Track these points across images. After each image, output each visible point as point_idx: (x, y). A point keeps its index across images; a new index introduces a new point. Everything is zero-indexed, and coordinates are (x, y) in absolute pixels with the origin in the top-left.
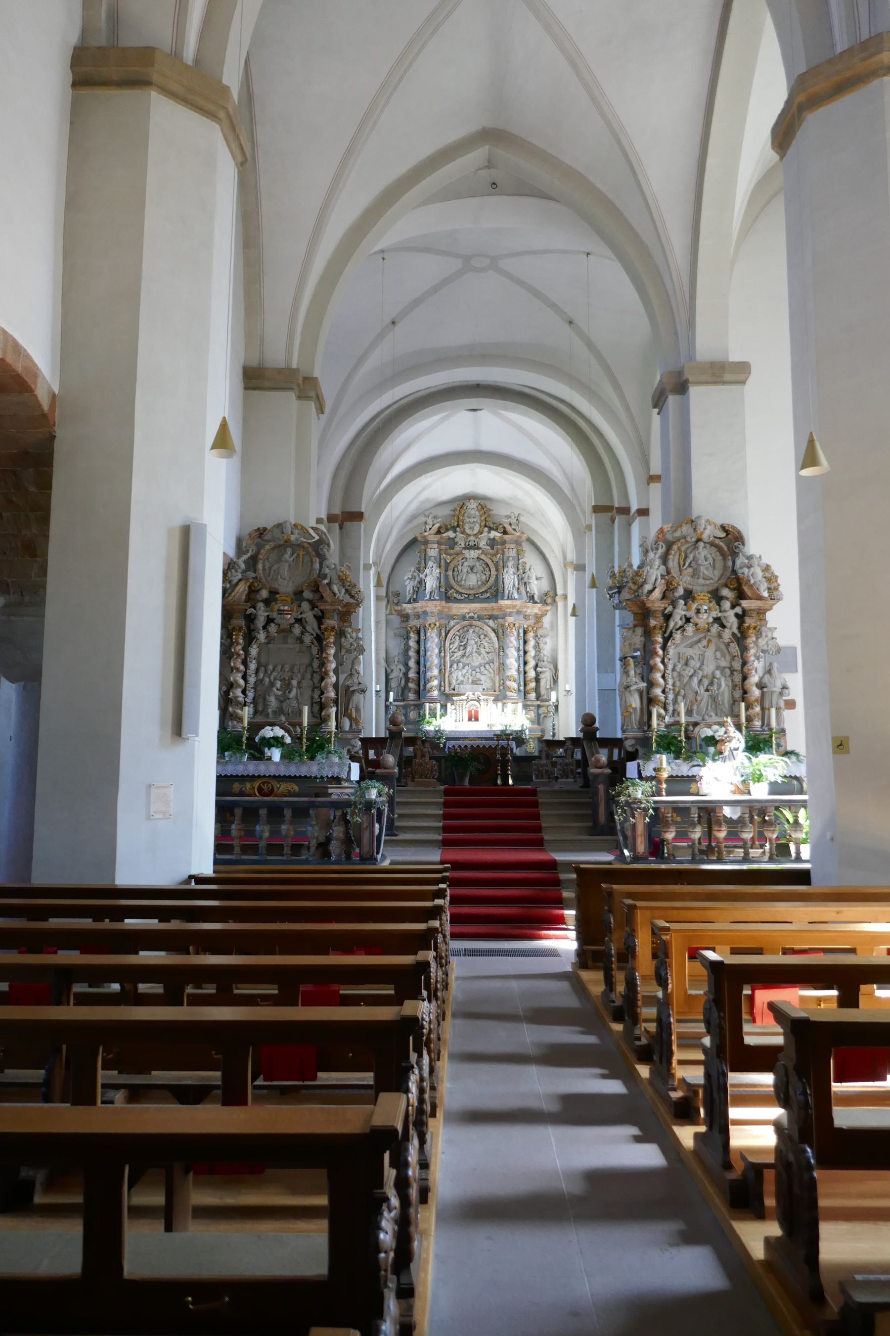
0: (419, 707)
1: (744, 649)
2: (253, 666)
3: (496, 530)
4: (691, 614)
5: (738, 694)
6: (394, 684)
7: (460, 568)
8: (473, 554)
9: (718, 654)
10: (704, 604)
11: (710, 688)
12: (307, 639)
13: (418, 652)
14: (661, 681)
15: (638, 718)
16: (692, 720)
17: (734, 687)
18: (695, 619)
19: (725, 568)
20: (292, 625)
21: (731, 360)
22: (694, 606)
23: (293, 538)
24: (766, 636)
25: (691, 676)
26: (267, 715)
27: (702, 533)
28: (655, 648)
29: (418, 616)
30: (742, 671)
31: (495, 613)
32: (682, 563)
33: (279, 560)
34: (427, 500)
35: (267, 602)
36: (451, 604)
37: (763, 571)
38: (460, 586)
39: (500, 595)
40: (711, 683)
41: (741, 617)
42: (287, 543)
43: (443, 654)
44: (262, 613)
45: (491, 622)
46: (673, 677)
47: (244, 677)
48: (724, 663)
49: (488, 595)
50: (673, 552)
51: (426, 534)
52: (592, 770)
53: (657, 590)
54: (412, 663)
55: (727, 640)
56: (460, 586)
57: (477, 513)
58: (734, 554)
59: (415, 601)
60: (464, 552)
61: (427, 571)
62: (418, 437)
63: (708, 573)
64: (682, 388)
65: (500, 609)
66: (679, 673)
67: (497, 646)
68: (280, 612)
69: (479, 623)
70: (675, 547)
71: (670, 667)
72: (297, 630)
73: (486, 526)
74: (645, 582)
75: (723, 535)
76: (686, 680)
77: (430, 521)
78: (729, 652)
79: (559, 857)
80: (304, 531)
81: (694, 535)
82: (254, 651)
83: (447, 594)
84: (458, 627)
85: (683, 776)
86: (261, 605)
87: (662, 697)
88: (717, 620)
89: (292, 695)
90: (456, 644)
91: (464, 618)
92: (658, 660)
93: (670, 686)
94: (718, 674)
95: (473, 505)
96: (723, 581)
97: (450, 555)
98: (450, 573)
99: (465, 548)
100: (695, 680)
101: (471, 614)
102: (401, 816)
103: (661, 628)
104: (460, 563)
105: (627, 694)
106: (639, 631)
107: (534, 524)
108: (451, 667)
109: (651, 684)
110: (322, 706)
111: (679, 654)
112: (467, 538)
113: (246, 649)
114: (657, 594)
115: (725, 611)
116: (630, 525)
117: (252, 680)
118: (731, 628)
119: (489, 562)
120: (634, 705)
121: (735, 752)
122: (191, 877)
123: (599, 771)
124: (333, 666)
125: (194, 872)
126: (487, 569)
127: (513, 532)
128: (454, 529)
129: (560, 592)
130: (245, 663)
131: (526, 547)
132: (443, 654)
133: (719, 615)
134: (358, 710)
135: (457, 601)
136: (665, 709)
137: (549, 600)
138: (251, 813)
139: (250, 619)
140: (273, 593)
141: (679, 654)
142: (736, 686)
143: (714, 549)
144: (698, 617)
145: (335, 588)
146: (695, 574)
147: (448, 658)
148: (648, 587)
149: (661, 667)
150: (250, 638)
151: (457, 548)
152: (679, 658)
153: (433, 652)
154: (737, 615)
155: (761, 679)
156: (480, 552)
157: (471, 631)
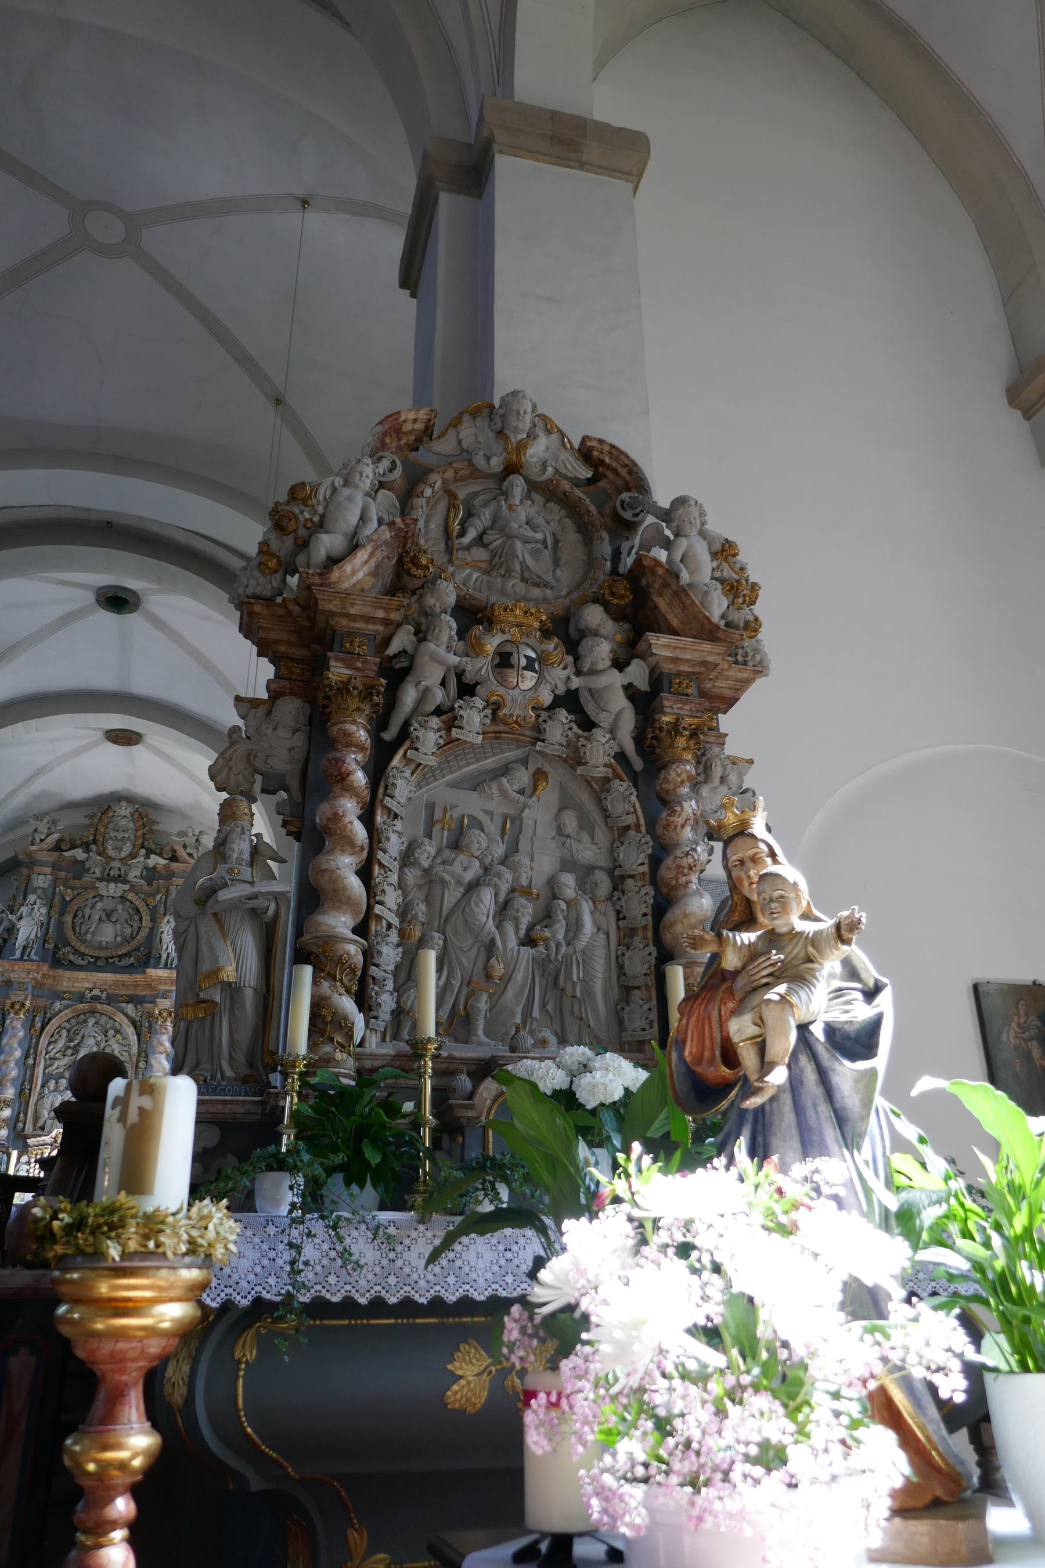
1: (659, 803)
3: (160, 855)
4: (480, 667)
7: (87, 911)
8: (113, 889)
9: (570, 821)
10: (518, 633)
11: (539, 932)
14: (355, 884)
15: (244, 1036)
17: (626, 935)
18: (492, 687)
19: (591, 562)
21: (596, 118)
22: (492, 643)
24: (723, 780)
25: (473, 887)
27: (522, 446)
28: (340, 762)
30: (654, 878)
31: (140, 992)
32: (456, 528)
34: (44, 794)
36: (60, 972)
37: (714, 555)
38: (84, 942)
39: (152, 961)
40: (546, 917)
41: (644, 702)
43: (31, 1061)
45: (130, 1009)
46: (401, 885)
48: (589, 851)
49: (132, 960)
50: (428, 492)
51: (34, 848)
53: (361, 556)
55: (602, 772)
56: (84, 942)
57: (131, 825)
60: (98, 884)
61: (24, 910)
63: (541, 567)
64: (474, 175)
65: (149, 985)
66: (427, 872)
67: (135, 1050)
69: (108, 1008)
73: (143, 847)
74: (321, 526)
75: (586, 473)
76: (451, 897)
77: (43, 828)
78: (606, 815)
81: (497, 448)
83: (56, 952)
84: (68, 1013)
85: (408, 1306)
87: (353, 950)
88: (569, 701)
90: (61, 1044)
91: (81, 998)
92: (350, 808)
94: (568, 881)
95: (124, 809)
97: (73, 889)
98: (68, 919)
99: (101, 880)
100: (487, 900)
101: (97, 992)
103: (367, 693)
104: (89, 904)
105: (208, 927)
108: (43, 1086)
111: (431, 807)
112: (107, 863)
114: (358, 571)
115: (593, 672)
118: (613, 731)
120: (229, 973)
121: (846, 1072)
126: (136, 917)
127: (188, 858)
128: (86, 846)
132: (31, 1061)
133: (576, 683)
135: (73, 966)
141: (431, 807)
142: (632, 932)
143: (556, 511)
144: (502, 681)
146: (498, 563)
147: (40, 1070)
148: (327, 543)
149: (360, 832)
151: (87, 878)
152: (431, 823)
153: (10, 1054)
154: (630, 690)
156: (127, 887)
157: (91, 1021)
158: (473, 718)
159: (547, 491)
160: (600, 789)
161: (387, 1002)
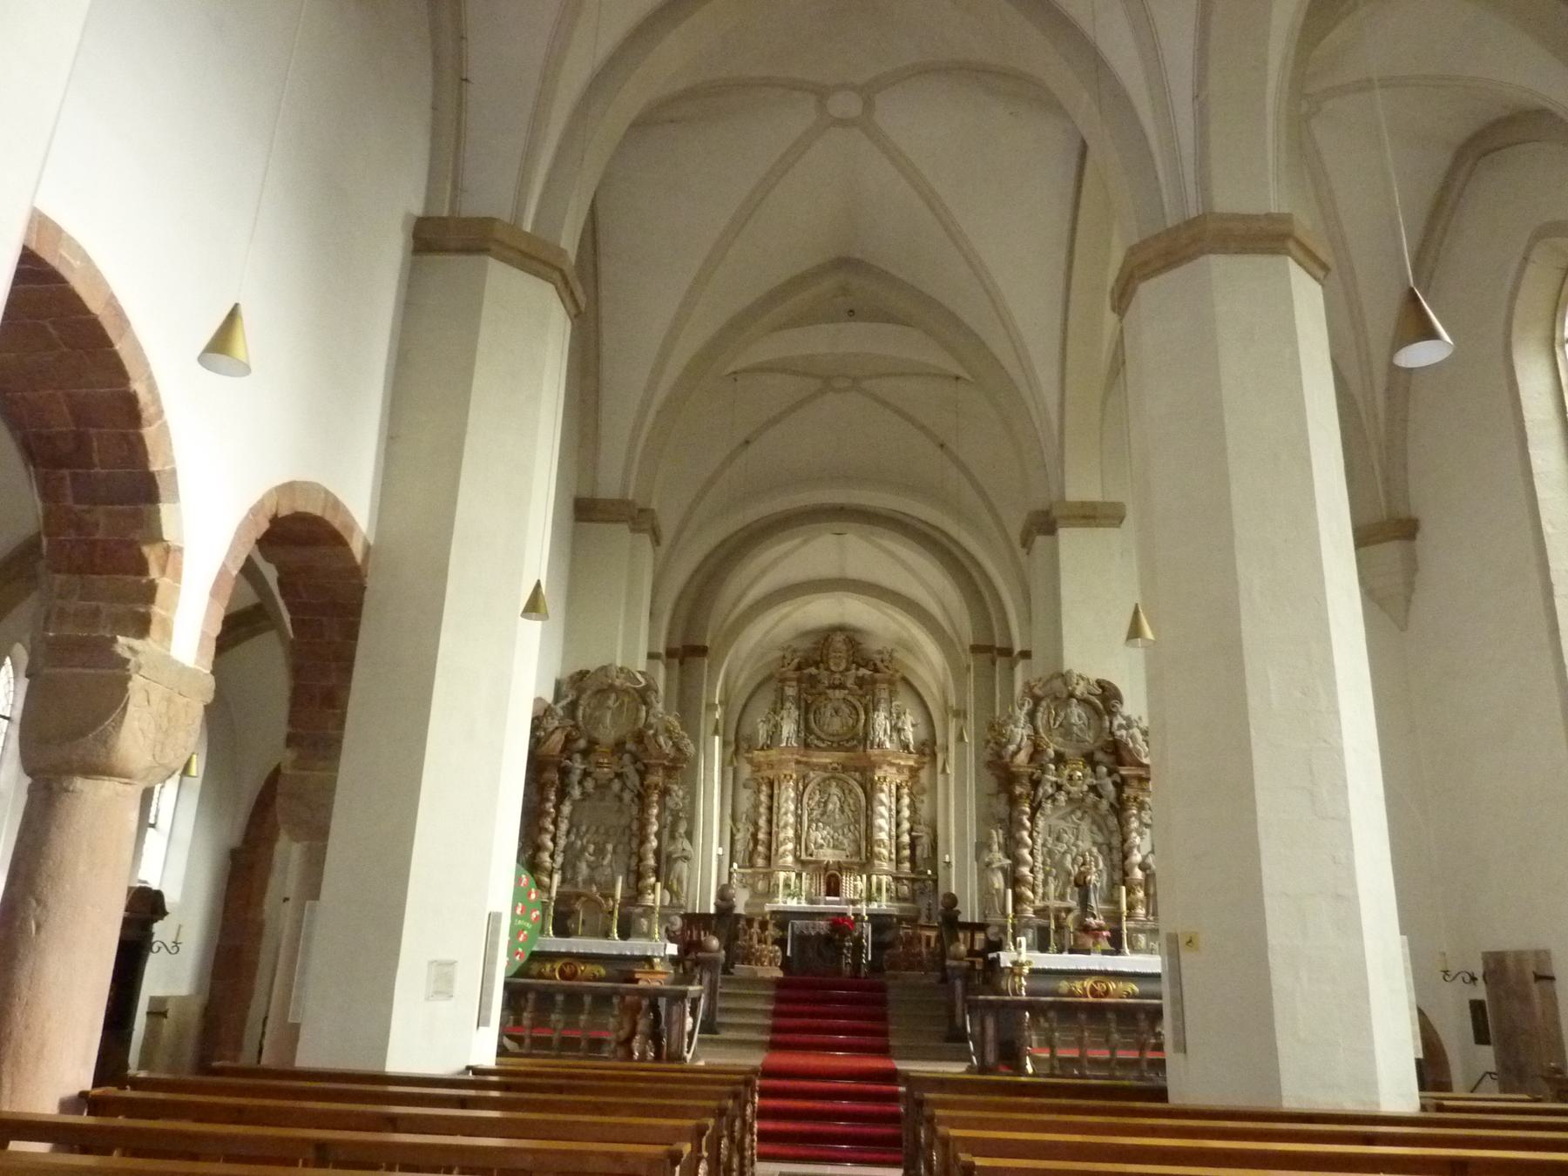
0: (768, 876)
1: (1123, 824)
2: (564, 826)
5: (1117, 876)
6: (739, 847)
8: (839, 694)
12: (627, 796)
13: (770, 809)
14: (1029, 858)
16: (1064, 905)
18: (1068, 786)
20: (611, 780)
23: (618, 683)
25: (1064, 853)
26: (576, 885)
29: (771, 766)
33: (601, 705)
35: (585, 753)
41: (1120, 786)
42: (612, 687)
44: (578, 765)
47: (554, 840)
52: (948, 962)
54: (762, 822)
58: (1112, 713)
59: (769, 747)
61: (784, 713)
62: (774, 563)
68: (599, 765)
70: (1044, 703)
71: (1040, 841)
72: (616, 786)
74: (1009, 742)
75: (1099, 691)
77: (789, 656)
79: (902, 1066)
80: (630, 676)
82: (566, 809)
86: (577, 757)
87: (1030, 878)
89: (606, 862)
92: (1025, 834)
93: (1039, 865)
95: (839, 638)
96: (1098, 744)
102: (727, 1011)
106: (1003, 797)
107: (909, 660)
109: (1017, 861)
110: (640, 876)
113: (557, 807)
114: (1022, 758)
116: (1012, 668)
117: (562, 842)
119: (858, 704)
122: (468, 1068)
123: (954, 963)
124: (655, 828)
125: (472, 1063)
128: (817, 664)
129: (939, 741)
130: (555, 823)
131: (901, 688)
134: (680, 882)
136: (1034, 892)
137: (927, 751)
138: (545, 998)
139: (565, 772)
140: (593, 743)
145: (661, 740)
147: (805, 818)
148: (1012, 748)
149: (1029, 841)
150: (562, 794)
151: (820, 688)
154: (1115, 783)
155: (1145, 858)
158: (1062, 797)
159: (1083, 701)
160: (1104, 818)
161: (1040, 891)
